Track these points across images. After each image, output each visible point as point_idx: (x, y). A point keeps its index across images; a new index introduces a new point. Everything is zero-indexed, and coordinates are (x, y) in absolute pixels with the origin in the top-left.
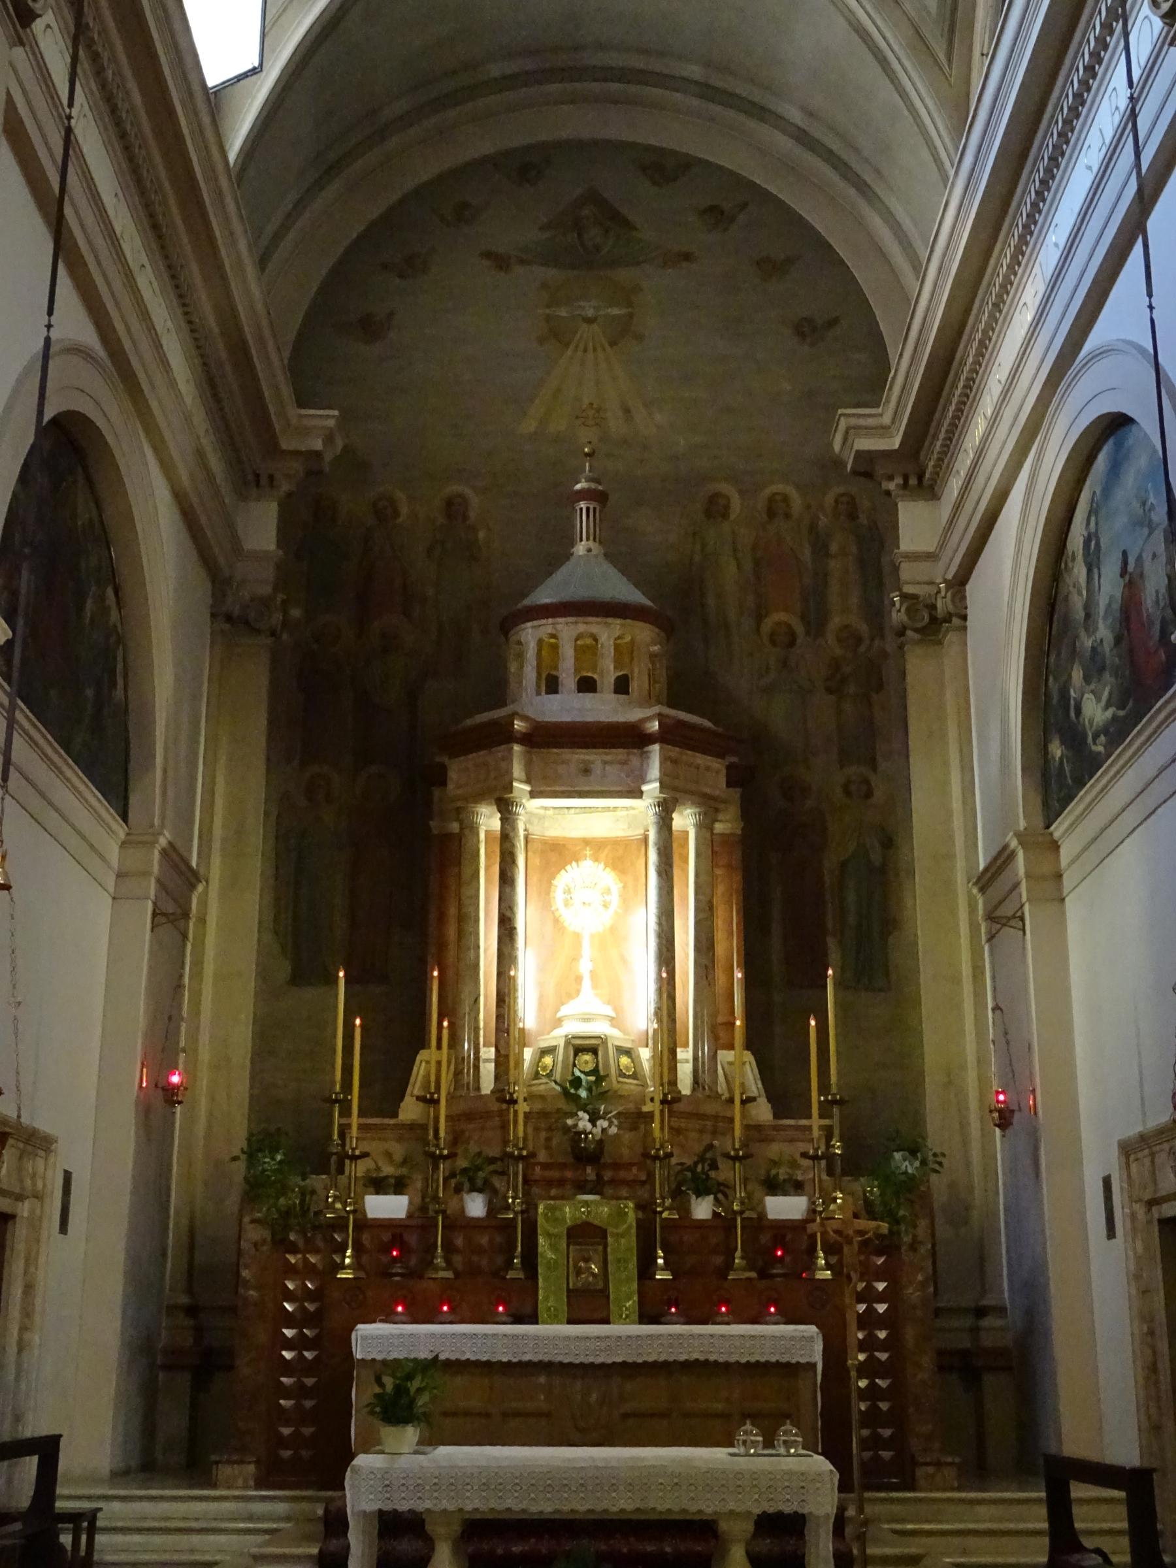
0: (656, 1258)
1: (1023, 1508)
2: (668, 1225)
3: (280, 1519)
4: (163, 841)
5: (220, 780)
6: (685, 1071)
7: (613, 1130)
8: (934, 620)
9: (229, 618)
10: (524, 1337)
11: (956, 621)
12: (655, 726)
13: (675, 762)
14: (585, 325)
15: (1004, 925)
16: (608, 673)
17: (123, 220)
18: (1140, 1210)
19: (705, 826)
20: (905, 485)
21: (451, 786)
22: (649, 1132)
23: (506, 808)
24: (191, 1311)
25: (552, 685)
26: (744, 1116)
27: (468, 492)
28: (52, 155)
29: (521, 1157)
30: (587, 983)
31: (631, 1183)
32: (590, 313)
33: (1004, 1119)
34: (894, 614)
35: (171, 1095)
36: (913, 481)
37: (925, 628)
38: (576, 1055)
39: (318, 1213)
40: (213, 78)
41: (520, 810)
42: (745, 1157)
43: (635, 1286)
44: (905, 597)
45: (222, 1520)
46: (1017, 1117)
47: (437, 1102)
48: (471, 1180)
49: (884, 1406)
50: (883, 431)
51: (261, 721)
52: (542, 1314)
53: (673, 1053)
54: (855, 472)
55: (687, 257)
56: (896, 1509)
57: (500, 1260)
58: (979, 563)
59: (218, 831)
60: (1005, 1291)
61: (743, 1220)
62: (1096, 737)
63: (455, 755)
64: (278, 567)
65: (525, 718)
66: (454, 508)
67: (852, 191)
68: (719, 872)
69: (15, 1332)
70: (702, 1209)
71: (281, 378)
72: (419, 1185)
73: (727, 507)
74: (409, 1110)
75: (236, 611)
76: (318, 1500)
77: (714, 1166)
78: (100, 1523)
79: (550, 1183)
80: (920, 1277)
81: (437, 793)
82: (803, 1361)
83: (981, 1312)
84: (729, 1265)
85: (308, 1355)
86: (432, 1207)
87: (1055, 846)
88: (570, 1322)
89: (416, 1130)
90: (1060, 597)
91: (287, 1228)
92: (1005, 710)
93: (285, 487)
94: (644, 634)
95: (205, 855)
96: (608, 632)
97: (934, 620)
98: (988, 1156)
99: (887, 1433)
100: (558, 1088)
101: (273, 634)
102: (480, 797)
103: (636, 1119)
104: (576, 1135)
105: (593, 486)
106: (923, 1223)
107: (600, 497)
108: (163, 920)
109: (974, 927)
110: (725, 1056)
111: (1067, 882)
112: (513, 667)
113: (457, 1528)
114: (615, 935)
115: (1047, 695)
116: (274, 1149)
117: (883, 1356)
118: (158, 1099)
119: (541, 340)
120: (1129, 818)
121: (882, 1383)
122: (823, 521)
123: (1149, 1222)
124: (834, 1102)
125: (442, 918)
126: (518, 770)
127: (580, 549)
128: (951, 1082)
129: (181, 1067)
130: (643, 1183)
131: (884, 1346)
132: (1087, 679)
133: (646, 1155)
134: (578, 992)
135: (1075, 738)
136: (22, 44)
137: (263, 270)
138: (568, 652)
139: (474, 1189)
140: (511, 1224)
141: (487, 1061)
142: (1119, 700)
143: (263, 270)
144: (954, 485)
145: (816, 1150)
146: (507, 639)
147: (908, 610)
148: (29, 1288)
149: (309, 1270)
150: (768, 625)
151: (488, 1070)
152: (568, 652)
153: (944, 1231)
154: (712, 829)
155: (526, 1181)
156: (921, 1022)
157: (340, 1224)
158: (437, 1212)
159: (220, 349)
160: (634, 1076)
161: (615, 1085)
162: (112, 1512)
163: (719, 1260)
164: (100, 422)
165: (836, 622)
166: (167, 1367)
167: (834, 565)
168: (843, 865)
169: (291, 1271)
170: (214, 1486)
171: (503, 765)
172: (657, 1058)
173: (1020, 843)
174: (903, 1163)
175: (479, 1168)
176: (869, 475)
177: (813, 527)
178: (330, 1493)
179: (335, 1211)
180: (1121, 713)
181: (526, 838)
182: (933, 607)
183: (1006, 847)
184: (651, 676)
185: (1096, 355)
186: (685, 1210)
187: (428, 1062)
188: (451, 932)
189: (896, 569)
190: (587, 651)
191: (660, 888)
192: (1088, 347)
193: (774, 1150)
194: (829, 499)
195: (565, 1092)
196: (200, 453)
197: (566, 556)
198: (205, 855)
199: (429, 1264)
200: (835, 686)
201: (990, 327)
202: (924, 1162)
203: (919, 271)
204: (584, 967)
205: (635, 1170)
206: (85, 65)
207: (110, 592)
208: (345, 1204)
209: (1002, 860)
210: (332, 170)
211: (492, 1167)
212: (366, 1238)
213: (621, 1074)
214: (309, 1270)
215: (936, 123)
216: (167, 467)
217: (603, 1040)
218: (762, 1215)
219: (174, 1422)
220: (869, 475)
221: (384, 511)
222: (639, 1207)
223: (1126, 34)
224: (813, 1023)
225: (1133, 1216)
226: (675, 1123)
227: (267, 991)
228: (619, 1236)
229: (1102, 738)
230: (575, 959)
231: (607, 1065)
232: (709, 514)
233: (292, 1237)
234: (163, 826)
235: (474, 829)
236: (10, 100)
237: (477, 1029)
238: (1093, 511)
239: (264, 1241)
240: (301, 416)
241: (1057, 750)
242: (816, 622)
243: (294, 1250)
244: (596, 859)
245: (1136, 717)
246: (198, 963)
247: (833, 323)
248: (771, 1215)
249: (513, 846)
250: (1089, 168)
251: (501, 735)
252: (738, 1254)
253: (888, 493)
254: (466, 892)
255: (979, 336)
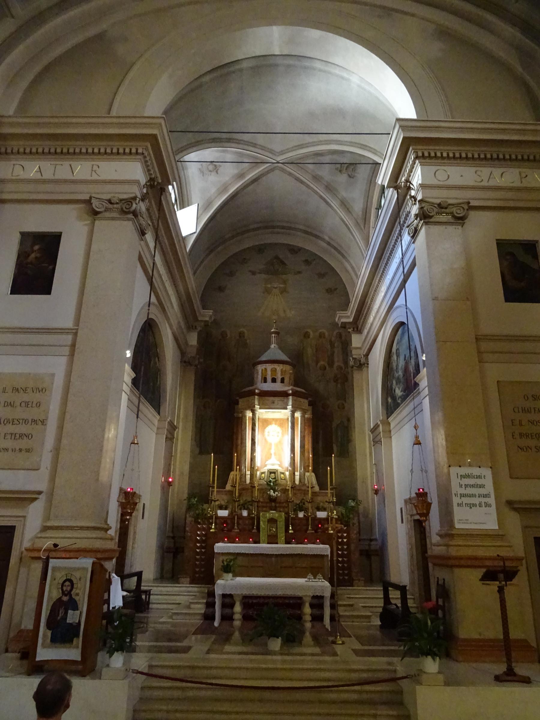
0: (289, 527)
1: (366, 600)
2: (292, 518)
3: (195, 592)
4: (168, 420)
5: (182, 402)
6: (297, 478)
7: (279, 495)
8: (360, 364)
9: (185, 362)
10: (257, 547)
11: (366, 365)
12: (291, 392)
13: (295, 400)
14: (274, 289)
15: (376, 443)
16: (279, 377)
17: (165, 277)
18: (409, 516)
19: (303, 417)
20: (353, 330)
21: (240, 406)
22: (288, 494)
23: (253, 412)
24: (173, 538)
25: (265, 381)
26: (311, 490)
27: (246, 331)
28: (150, 266)
29: (256, 501)
30: (273, 456)
31: (284, 507)
32: (275, 286)
33: (376, 492)
34: (351, 363)
35: (170, 484)
36: (356, 329)
37: (358, 366)
38: (270, 474)
39: (206, 515)
40: (184, 234)
41: (257, 412)
42: (311, 502)
43: (284, 535)
44: (353, 358)
45: (181, 592)
46: (379, 492)
47: (236, 487)
48: (244, 507)
49: (346, 565)
50: (348, 317)
51: (192, 387)
52: (261, 541)
53: (294, 474)
54: (341, 327)
55: (299, 272)
56: (348, 591)
57: (251, 527)
58: (372, 350)
59: (182, 416)
60: (377, 536)
61: (311, 518)
62: (399, 398)
63: (241, 398)
64: (197, 349)
65: (258, 389)
66: (241, 335)
67: (341, 257)
68: (306, 427)
69: (131, 544)
70: (301, 515)
71: (199, 302)
72: (231, 507)
73: (309, 335)
74: (228, 487)
75: (187, 360)
76: (206, 587)
77: (304, 504)
78: (151, 593)
79: (263, 507)
80: (355, 532)
81: (236, 407)
82: (326, 554)
83: (371, 540)
84: (307, 529)
85: (203, 550)
86: (234, 513)
87: (389, 424)
88: (268, 543)
89: (231, 493)
90: (391, 362)
91: (198, 518)
92: (377, 388)
93: (199, 329)
94: (288, 368)
95: (178, 422)
96: (279, 368)
97: (360, 364)
98: (373, 500)
99: (346, 572)
100: (266, 483)
101: (196, 366)
102: (246, 409)
103: (285, 491)
104: (270, 496)
105: (276, 330)
106: (356, 518)
107: (277, 333)
108: (168, 439)
109: (370, 444)
110: (307, 474)
111: (392, 433)
112: (256, 375)
113: (241, 598)
114: (280, 442)
115: (387, 386)
116: (195, 498)
117: (346, 553)
118: (166, 484)
119: (264, 293)
120: (406, 420)
121: (345, 559)
122: (333, 339)
123: (411, 521)
124: (334, 488)
125: (237, 439)
126: (256, 402)
127: (272, 346)
128: (364, 482)
129: (171, 476)
130: (286, 507)
131: (346, 550)
132: (397, 384)
133: (287, 501)
134: (271, 458)
135: (394, 398)
136: (143, 240)
137: (194, 275)
138: (269, 372)
139: (244, 509)
140: (253, 518)
141: (248, 475)
142: (404, 390)
143: (194, 275)
144: (365, 331)
145: (329, 500)
146: (254, 368)
147: (354, 362)
148: (135, 533)
149: (204, 529)
150: (319, 365)
151: (248, 477)
152: (269, 372)
153: (362, 519)
154: (304, 417)
155: (257, 506)
156: (357, 466)
157: (211, 517)
158: (235, 515)
159: (184, 297)
160: (285, 479)
161: (280, 482)
162: (154, 590)
163: (305, 528)
164: (157, 321)
165: (336, 364)
166: (167, 552)
167: (336, 350)
168: (338, 425)
169: (199, 529)
170: (179, 583)
171: (253, 401)
172: (290, 474)
173: (381, 423)
174: (352, 503)
175: (246, 504)
176: (345, 327)
177: (331, 341)
178: (209, 586)
179: (210, 514)
180: (404, 394)
181: (258, 418)
182: (360, 361)
183: (377, 423)
184: (290, 379)
185: (397, 308)
186: (297, 515)
187: (233, 475)
188: (239, 442)
189: (351, 351)
190: (274, 371)
191: (291, 432)
192: (396, 304)
193: (319, 499)
194: (335, 333)
195: (267, 484)
196: (179, 323)
197: (269, 348)
198: (178, 422)
199: (233, 528)
200: (336, 380)
201: (374, 295)
202: (356, 503)
203: (358, 277)
204: (272, 451)
205: (284, 504)
206: (158, 245)
207: (157, 358)
208: (213, 513)
209: (376, 426)
210: (211, 251)
211: (249, 503)
212: (218, 521)
213: (282, 479)
214: (204, 529)
215: (361, 244)
216: (171, 328)
217: (277, 471)
218: (316, 516)
219: (168, 566)
220: (345, 327)
221: (224, 335)
222: (285, 513)
223: (401, 240)
224: (329, 468)
225: (407, 518)
226: (295, 491)
227: (193, 456)
228: (280, 522)
229: (400, 399)
230: (270, 449)
231: (278, 477)
232: (305, 336)
233: (199, 521)
234: (168, 416)
235: (245, 416)
236: (140, 252)
237: (245, 467)
238: (398, 343)
239: (192, 521)
240: (203, 312)
241: (390, 400)
242: (331, 363)
243: (199, 523)
244: (276, 424)
245: (407, 396)
246: (176, 450)
247: (336, 289)
248: (318, 516)
249: (255, 421)
250: (396, 263)
251: (252, 393)
252: (310, 526)
253: (349, 332)
254: (243, 432)
255: (371, 297)
